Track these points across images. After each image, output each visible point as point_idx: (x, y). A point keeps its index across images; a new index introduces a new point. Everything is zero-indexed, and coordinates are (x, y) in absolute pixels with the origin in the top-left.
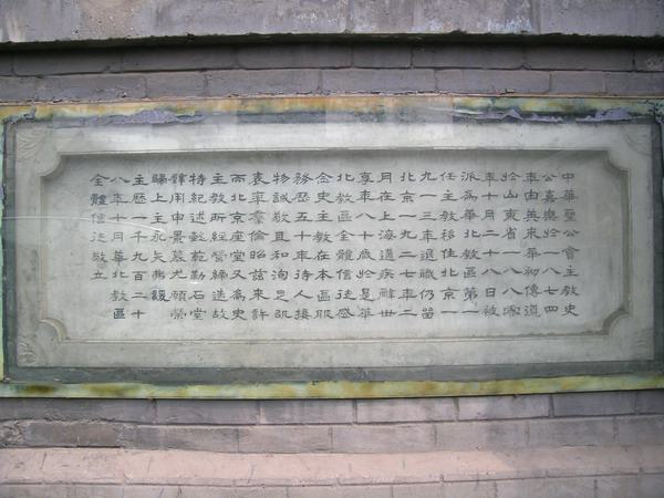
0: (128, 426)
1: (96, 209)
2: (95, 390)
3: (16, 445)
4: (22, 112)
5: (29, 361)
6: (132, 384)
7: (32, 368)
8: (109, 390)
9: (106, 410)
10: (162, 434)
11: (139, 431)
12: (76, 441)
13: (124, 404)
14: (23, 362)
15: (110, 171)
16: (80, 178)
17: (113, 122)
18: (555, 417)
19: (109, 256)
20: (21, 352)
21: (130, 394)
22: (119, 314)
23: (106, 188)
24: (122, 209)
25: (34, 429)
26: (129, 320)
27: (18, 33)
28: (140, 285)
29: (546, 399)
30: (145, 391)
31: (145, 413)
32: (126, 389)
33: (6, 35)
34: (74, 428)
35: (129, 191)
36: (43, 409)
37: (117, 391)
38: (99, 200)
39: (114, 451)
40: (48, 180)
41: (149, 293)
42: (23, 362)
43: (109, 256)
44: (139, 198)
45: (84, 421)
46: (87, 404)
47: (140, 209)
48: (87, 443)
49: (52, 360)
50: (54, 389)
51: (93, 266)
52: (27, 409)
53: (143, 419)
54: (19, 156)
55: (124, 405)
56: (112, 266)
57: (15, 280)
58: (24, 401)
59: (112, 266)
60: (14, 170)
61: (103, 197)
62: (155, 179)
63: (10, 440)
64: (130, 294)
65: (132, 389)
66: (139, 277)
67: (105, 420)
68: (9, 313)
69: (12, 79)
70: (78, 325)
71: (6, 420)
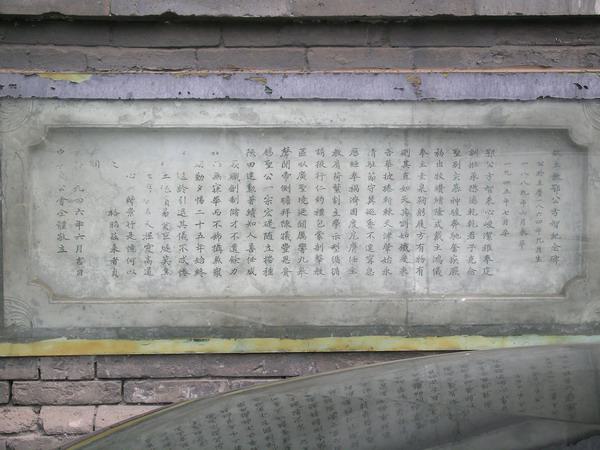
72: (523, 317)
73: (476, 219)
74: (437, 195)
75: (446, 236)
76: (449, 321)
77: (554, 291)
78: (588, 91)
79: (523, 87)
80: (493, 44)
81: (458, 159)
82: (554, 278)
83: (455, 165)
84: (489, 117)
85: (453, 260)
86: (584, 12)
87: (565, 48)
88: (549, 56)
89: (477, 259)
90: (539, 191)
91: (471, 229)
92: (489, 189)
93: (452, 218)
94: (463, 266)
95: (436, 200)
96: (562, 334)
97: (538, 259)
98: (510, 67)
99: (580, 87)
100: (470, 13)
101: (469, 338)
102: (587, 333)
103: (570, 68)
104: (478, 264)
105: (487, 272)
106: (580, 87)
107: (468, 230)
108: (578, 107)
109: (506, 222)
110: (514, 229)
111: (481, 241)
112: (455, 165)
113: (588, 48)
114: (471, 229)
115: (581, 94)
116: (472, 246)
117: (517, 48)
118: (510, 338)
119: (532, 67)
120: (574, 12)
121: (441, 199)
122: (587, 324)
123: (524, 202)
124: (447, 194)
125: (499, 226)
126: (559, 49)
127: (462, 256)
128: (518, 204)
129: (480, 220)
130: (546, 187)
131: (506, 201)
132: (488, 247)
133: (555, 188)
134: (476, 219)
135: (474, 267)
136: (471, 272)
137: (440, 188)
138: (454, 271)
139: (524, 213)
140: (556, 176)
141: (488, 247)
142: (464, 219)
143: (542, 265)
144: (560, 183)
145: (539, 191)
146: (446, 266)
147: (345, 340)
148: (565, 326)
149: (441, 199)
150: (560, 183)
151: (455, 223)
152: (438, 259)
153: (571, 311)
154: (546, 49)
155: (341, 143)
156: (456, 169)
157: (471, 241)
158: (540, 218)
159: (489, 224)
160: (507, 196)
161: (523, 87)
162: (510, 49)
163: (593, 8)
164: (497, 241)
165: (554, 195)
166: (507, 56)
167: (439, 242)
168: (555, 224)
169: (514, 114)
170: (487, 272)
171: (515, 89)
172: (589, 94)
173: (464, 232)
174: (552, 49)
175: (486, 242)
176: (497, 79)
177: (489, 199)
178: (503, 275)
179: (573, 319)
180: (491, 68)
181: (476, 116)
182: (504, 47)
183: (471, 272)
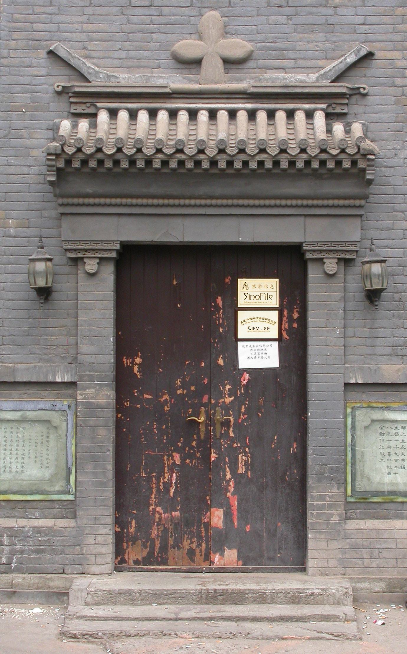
0: (394, 512)
1: (381, 438)
2: (383, 499)
3: (353, 519)
4: (359, 405)
5: (360, 489)
6: (396, 497)
7: (360, 492)
8: (388, 499)
9: (386, 506)
10: (405, 514)
11: (398, 513)
12: (374, 517)
13: (393, 503)
14: (358, 490)
15: (387, 425)
16: (377, 426)
17: (388, 408)
18: (289, 7)
19: (386, 454)
20: (357, 486)
21: (395, 500)
22: (389, 473)
23: (385, 430)
24: (390, 438)
25: (360, 513)
26: (393, 475)
27: (360, 380)
28: (397, 464)
29: (328, 57)
30: (400, 499)
31: (399, 506)
32: (394, 499)
33: (356, 380)
34: (374, 512)
35: (394, 431)
36: (363, 506)
37: (391, 499)
38: (382, 434)
39: (389, 520)
40: (366, 428)
41: (400, 466)
42: (358, 490)
43: (386, 454)
44: (397, 434)
45: (378, 510)
46: (379, 504)
47: (397, 438)
48: (379, 518)
49: (368, 489)
50: (369, 499)
51: (380, 457)
52: (358, 505)
53: (399, 509)
54: (356, 419)
55: (392, 504)
56: (387, 457)
57: (355, 462)
58: (357, 503)
59: (387, 457)
60: (355, 424)
61: (384, 433)
62: (402, 427)
63: (351, 517)
64: (393, 467)
65: (396, 498)
66: (396, 461)
67: (385, 509)
68: (353, 473)
69: (354, 393)
70: (376, 478)
71: (350, 510)
72: (34, 488)
73: (18, 452)
74: (4, 443)
75: (7, 458)
76: (7, 489)
77: (47, 479)
78: (57, 407)
79: (33, 405)
80: (23, 390)
81: (12, 430)
82: (47, 474)
83: (11, 432)
84: (22, 416)
85: (10, 467)
86: (52, 381)
87: (49, 392)
88: (43, 394)
89: (19, 467)
90: (42, 442)
91: (17, 456)
92: (23, 441)
93: (10, 452)
94: (14, 470)
95: (4, 445)
96: (48, 494)
97: (42, 467)
98: (30, 398)
99: (54, 406)
100: (13, 381)
101: (14, 495)
102: (57, 494)
103: (51, 398)
104: (19, 469)
105: (22, 472)
106: (54, 406)
107: (15, 457)
108: (54, 412)
109: (29, 453)
110: (33, 456)
111: (20, 460)
112: (11, 432)
113: (57, 391)
114: (17, 456)
115: (54, 408)
116: (17, 462)
117: (32, 391)
118: (28, 496)
119: (37, 398)
120: (49, 380)
121: (6, 445)
122: (57, 491)
123: (36, 446)
124: (8, 443)
125: (27, 455)
126: (47, 392)
127: (13, 466)
128: (34, 447)
129: (20, 453)
130: (45, 441)
131: (30, 446)
132: (23, 463)
133: (48, 441)
134: (18, 452)
135: (18, 470)
136: (17, 472)
137: (6, 441)
138: (10, 471)
139: (37, 450)
140: (48, 437)
141: (23, 463)
142: (14, 452)
143: (43, 470)
144: (50, 440)
145: (42, 442)
146: (7, 470)
147: (170, 587)
148: (49, 492)
149: (6, 445)
150: (50, 440)
151: (11, 454)
152: (5, 467)
153: (51, 486)
154: (43, 392)
155: (220, 29)
156: (12, 434)
157: (17, 460)
158: (42, 452)
159: (23, 454)
160: (30, 444)
161: (33, 405)
162: (29, 392)
163: (55, 379)
164: (26, 460)
165: (47, 444)
166: (28, 394)
167: (5, 460)
168: (48, 454)
169: (30, 415)
170: (22, 472)
171: (31, 406)
172: (57, 408)
173: (14, 457)
174: (44, 392)
175: (22, 461)
176: (24, 403)
177: (23, 445)
178: (28, 473)
179: (52, 489)
180: (23, 399)
181: (16, 415)
182: (27, 391)
183: (17, 472)
